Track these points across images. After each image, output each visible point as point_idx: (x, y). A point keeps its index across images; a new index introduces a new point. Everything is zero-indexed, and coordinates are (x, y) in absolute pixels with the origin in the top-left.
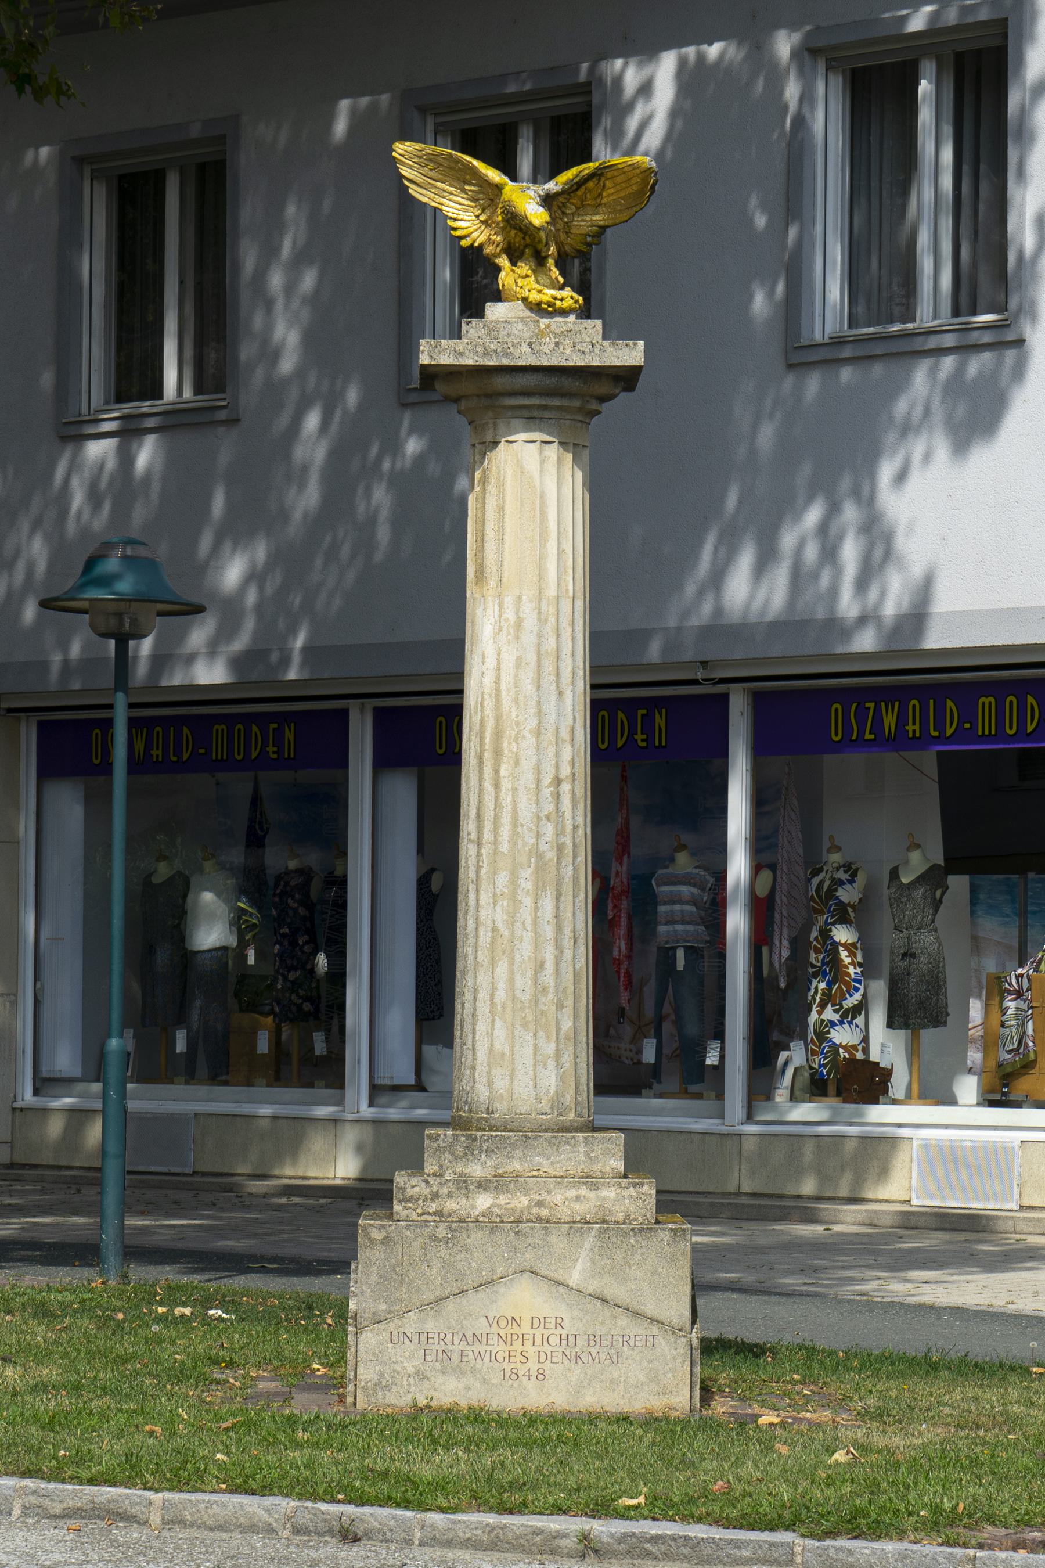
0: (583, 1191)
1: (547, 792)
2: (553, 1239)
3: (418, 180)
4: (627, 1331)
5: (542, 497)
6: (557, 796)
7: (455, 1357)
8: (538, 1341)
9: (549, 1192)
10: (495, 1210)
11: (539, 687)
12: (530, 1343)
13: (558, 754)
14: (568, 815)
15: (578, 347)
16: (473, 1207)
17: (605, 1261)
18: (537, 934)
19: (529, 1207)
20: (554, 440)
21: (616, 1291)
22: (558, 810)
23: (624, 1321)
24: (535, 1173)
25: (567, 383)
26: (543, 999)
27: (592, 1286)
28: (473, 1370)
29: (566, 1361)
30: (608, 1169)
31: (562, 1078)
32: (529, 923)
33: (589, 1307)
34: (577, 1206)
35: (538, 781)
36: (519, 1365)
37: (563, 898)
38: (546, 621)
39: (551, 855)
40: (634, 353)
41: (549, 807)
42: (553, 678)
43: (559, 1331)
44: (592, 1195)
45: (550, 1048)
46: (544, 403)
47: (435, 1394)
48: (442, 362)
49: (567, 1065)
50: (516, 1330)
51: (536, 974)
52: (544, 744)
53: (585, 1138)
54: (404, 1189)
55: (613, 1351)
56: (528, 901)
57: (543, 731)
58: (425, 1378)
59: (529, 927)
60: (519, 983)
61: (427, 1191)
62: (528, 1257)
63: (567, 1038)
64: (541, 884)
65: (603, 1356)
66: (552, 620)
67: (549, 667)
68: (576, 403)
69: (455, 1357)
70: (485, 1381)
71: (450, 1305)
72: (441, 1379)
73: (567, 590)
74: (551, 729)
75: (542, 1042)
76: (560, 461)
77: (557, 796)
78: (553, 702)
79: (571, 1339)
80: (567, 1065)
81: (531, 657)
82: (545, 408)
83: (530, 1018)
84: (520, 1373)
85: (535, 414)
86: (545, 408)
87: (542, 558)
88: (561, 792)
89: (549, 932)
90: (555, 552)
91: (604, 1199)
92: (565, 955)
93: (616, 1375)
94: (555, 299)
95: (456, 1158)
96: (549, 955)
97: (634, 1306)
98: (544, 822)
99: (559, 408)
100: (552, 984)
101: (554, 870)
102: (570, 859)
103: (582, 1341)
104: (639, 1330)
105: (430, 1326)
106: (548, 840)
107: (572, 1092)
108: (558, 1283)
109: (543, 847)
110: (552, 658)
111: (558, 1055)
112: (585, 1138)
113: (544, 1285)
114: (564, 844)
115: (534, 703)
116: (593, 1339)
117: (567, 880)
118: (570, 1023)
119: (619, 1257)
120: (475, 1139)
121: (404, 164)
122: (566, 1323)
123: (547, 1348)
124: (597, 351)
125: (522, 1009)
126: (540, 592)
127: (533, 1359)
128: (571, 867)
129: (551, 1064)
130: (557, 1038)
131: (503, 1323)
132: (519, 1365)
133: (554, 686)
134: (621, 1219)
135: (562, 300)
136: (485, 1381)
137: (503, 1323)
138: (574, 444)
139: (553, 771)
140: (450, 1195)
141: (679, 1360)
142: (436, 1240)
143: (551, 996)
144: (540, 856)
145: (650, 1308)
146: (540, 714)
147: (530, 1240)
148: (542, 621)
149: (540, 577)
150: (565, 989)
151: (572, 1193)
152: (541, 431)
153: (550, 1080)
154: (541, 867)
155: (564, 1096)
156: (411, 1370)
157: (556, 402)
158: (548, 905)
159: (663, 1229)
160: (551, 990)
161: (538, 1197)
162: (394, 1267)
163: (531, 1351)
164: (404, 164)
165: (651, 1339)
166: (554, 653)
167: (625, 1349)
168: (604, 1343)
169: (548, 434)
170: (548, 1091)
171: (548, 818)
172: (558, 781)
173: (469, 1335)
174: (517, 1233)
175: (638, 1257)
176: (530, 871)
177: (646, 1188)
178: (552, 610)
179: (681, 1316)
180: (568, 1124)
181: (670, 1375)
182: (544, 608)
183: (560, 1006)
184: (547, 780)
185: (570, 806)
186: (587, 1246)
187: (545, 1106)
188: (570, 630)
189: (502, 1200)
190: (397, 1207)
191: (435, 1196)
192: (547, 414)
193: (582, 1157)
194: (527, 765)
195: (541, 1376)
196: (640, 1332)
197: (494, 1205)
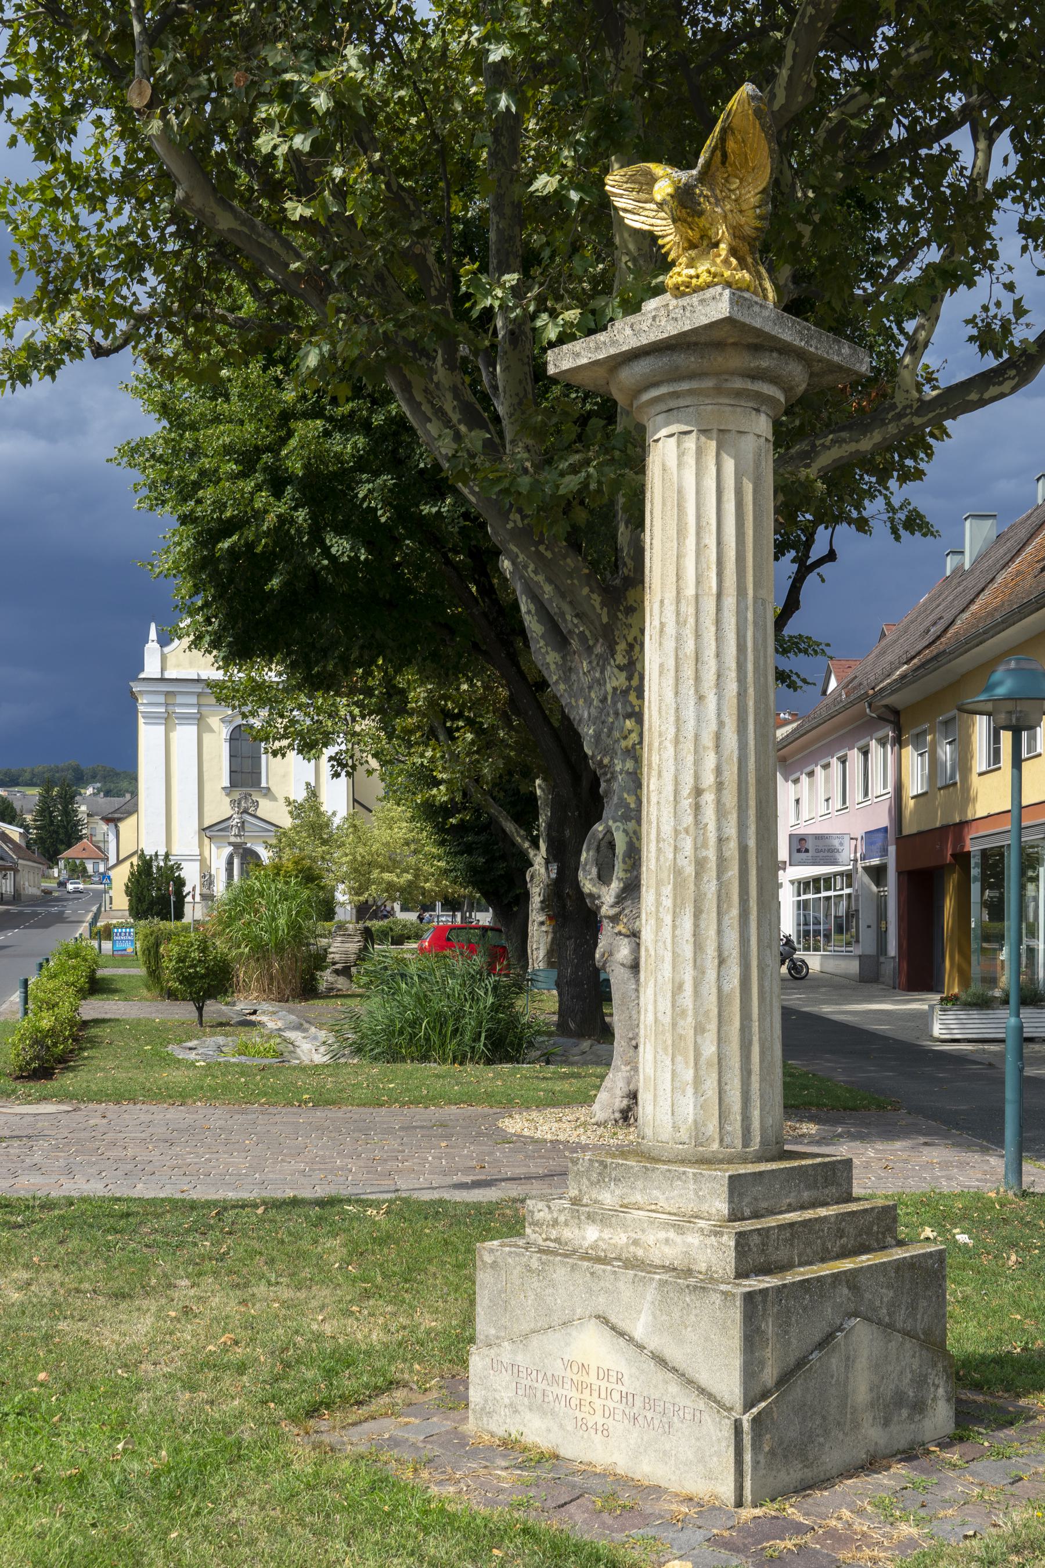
0: (672, 1234)
1: (686, 803)
2: (621, 1285)
3: (629, 207)
4: (678, 1400)
5: (680, 492)
6: (697, 808)
7: (539, 1395)
8: (603, 1395)
9: (643, 1231)
10: (600, 1243)
11: (677, 693)
12: (595, 1394)
13: (697, 762)
14: (712, 827)
15: (672, 315)
16: (584, 1238)
17: (664, 1317)
18: (675, 955)
19: (627, 1245)
20: (689, 428)
21: (674, 1354)
22: (697, 822)
23: (674, 1388)
24: (653, 1207)
25: (684, 360)
26: (681, 1023)
27: (653, 1343)
28: (553, 1412)
29: (626, 1421)
30: (714, 1211)
31: (702, 1107)
32: (669, 941)
33: (645, 1366)
34: (667, 1250)
35: (676, 792)
36: (587, 1415)
37: (704, 916)
38: (685, 622)
39: (690, 870)
40: (720, 305)
41: (688, 820)
42: (692, 682)
43: (619, 1387)
44: (678, 1239)
45: (688, 1075)
46: (671, 390)
47: (525, 1431)
48: (564, 368)
49: (710, 1093)
50: (585, 1378)
51: (673, 996)
52: (684, 753)
53: (694, 1174)
54: (533, 1212)
55: (665, 1420)
56: (668, 919)
57: (682, 739)
58: (516, 1411)
59: (669, 948)
60: (661, 1008)
61: (549, 1217)
62: (601, 1302)
63: (709, 1064)
64: (679, 901)
65: (656, 1422)
66: (691, 621)
67: (688, 672)
68: (709, 383)
69: (539, 1395)
70: (561, 1426)
71: (535, 1341)
72: (528, 1416)
73: (710, 588)
74: (691, 736)
75: (680, 1067)
76: (700, 452)
77: (697, 808)
78: (692, 708)
79: (630, 1397)
80: (710, 1093)
81: (671, 663)
82: (675, 395)
83: (669, 1042)
84: (590, 1425)
85: (672, 404)
86: (675, 395)
87: (679, 557)
88: (703, 803)
89: (688, 951)
90: (693, 547)
91: (689, 1245)
92: (707, 976)
93: (667, 1447)
94: (691, 277)
95: (592, 1184)
96: (688, 976)
97: (690, 1372)
98: (683, 835)
99: (690, 392)
100: (691, 1007)
101: (692, 887)
102: (714, 874)
103: (639, 1403)
104: (689, 1401)
105: (520, 1359)
106: (687, 854)
107: (715, 1120)
108: (622, 1334)
109: (682, 862)
110: (691, 662)
111: (697, 1081)
112: (694, 1174)
113: (608, 1333)
114: (705, 859)
115: (672, 711)
116: (649, 1403)
117: (709, 896)
118: (714, 1049)
119: (676, 1315)
120: (605, 1167)
121: (616, 195)
122: (625, 1379)
123: (610, 1404)
124: (688, 314)
125: (663, 1033)
126: (678, 593)
127: (599, 1412)
128: (715, 882)
129: (690, 1091)
130: (696, 1064)
131: (575, 1369)
132: (587, 1415)
133: (692, 692)
134: (703, 1270)
135: (698, 277)
136: (561, 1426)
137: (575, 1369)
138: (720, 431)
139: (692, 781)
140: (566, 1224)
141: (724, 1444)
142: (530, 1270)
143: (690, 1019)
144: (678, 872)
145: (704, 1378)
146: (678, 722)
147: (602, 1284)
148: (680, 623)
149: (678, 578)
150: (707, 1013)
151: (662, 1235)
152: (678, 422)
153: (688, 1107)
154: (679, 886)
155: (705, 1125)
156: (507, 1401)
157: (685, 386)
158: (687, 923)
159: (715, 1290)
160: (690, 1013)
161: (634, 1236)
162: (500, 1292)
163: (598, 1403)
164: (621, 196)
165: (697, 1413)
166: (693, 655)
167: (675, 1419)
168: (658, 1409)
169: (686, 424)
170: (685, 1120)
171: (687, 831)
172: (698, 792)
173: (549, 1375)
174: (592, 1274)
175: (692, 1318)
176: (670, 887)
177: (725, 1238)
178: (691, 610)
179: (732, 1393)
180: (708, 1156)
181: (715, 1459)
182: (683, 609)
183: (699, 1029)
184: (686, 790)
185: (713, 817)
186: (649, 1298)
187: (684, 1135)
188: (713, 629)
189: (606, 1234)
190: (528, 1231)
191: (555, 1223)
192: (682, 402)
193: (691, 1195)
194: (668, 777)
195: (605, 1432)
196: (689, 1404)
197: (600, 1239)
